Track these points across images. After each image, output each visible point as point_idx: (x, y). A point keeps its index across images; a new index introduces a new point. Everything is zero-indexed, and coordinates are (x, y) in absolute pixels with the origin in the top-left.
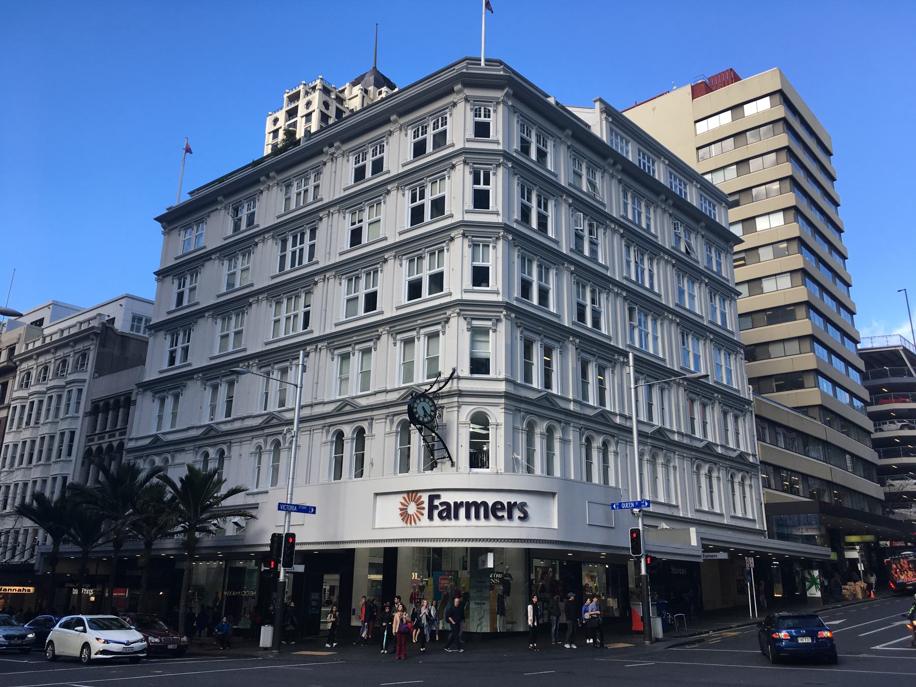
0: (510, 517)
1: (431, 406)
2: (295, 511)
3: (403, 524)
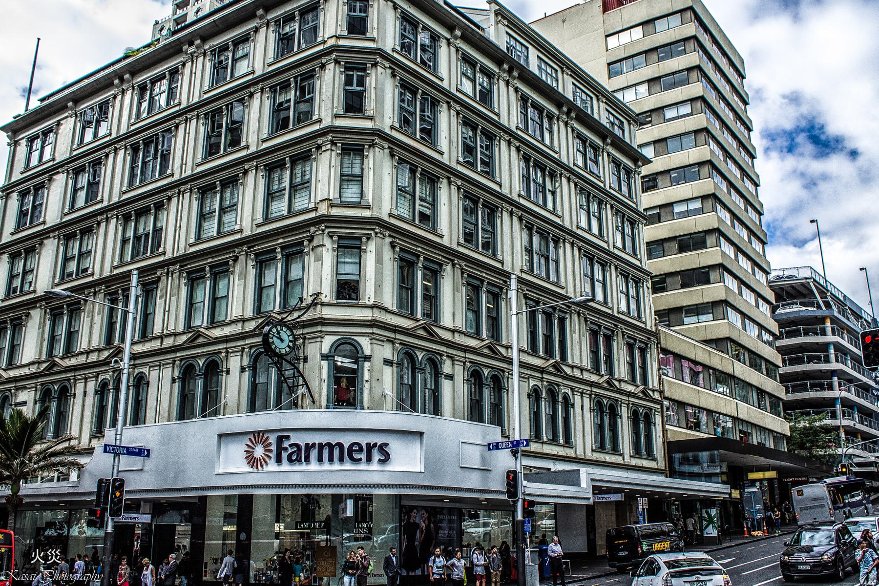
0: (369, 459)
1: (289, 336)
2: (125, 454)
3: (247, 469)
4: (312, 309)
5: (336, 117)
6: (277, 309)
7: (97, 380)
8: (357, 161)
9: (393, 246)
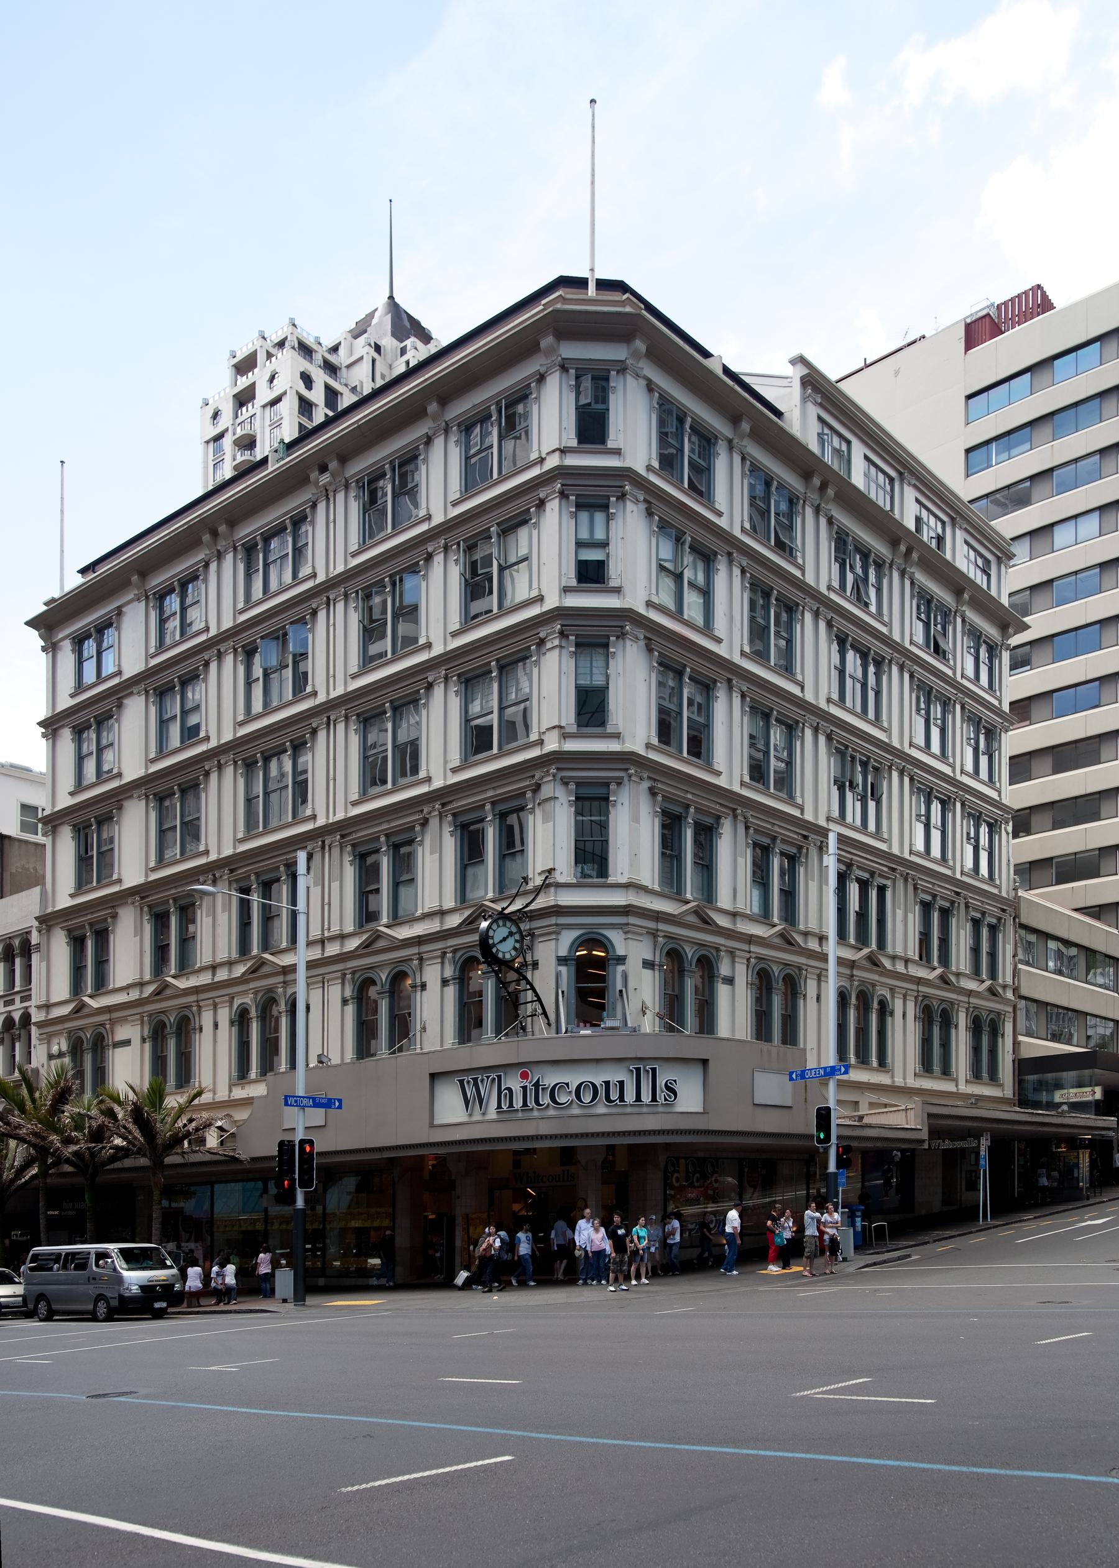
4: (542, 894)
5: (565, 591)
6: (490, 895)
7: (231, 1006)
8: (599, 661)
9: (653, 792)
